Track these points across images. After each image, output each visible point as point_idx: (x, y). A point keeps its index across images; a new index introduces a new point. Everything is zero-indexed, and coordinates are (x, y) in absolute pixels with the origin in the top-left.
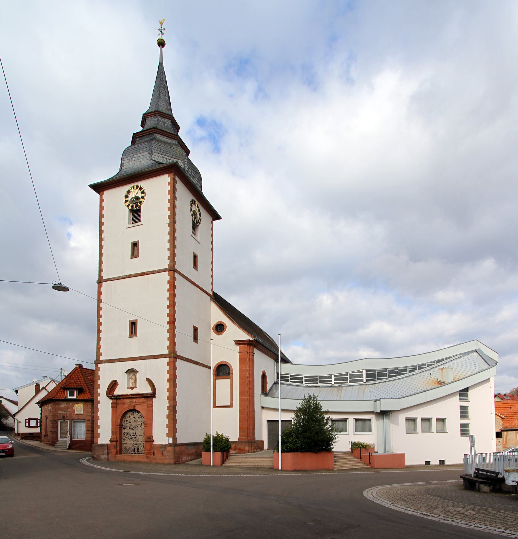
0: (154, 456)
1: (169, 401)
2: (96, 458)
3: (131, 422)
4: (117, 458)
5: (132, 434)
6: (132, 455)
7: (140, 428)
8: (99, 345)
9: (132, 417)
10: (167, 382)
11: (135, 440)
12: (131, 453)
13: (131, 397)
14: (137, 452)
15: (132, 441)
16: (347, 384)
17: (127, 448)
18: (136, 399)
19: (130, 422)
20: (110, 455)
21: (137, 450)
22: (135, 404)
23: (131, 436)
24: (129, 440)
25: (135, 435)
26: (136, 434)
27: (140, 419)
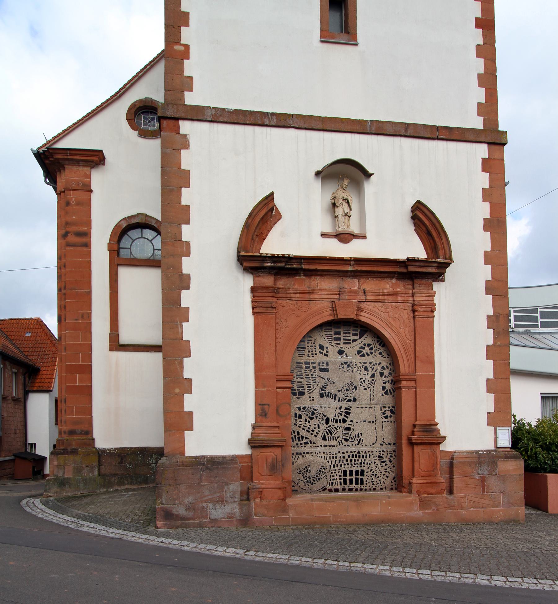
0: (451, 497)
2: (183, 519)
3: (326, 370)
4: (291, 514)
5: (331, 417)
6: (333, 499)
7: (368, 393)
8: (178, 42)
9: (333, 350)
11: (346, 440)
12: (330, 490)
13: (350, 268)
14: (354, 486)
15: (335, 443)
16: (538, 329)
17: (313, 472)
19: (321, 370)
20: (258, 500)
21: (354, 477)
22: (363, 297)
23: (327, 421)
24: (319, 440)
25: (344, 421)
26: (350, 417)
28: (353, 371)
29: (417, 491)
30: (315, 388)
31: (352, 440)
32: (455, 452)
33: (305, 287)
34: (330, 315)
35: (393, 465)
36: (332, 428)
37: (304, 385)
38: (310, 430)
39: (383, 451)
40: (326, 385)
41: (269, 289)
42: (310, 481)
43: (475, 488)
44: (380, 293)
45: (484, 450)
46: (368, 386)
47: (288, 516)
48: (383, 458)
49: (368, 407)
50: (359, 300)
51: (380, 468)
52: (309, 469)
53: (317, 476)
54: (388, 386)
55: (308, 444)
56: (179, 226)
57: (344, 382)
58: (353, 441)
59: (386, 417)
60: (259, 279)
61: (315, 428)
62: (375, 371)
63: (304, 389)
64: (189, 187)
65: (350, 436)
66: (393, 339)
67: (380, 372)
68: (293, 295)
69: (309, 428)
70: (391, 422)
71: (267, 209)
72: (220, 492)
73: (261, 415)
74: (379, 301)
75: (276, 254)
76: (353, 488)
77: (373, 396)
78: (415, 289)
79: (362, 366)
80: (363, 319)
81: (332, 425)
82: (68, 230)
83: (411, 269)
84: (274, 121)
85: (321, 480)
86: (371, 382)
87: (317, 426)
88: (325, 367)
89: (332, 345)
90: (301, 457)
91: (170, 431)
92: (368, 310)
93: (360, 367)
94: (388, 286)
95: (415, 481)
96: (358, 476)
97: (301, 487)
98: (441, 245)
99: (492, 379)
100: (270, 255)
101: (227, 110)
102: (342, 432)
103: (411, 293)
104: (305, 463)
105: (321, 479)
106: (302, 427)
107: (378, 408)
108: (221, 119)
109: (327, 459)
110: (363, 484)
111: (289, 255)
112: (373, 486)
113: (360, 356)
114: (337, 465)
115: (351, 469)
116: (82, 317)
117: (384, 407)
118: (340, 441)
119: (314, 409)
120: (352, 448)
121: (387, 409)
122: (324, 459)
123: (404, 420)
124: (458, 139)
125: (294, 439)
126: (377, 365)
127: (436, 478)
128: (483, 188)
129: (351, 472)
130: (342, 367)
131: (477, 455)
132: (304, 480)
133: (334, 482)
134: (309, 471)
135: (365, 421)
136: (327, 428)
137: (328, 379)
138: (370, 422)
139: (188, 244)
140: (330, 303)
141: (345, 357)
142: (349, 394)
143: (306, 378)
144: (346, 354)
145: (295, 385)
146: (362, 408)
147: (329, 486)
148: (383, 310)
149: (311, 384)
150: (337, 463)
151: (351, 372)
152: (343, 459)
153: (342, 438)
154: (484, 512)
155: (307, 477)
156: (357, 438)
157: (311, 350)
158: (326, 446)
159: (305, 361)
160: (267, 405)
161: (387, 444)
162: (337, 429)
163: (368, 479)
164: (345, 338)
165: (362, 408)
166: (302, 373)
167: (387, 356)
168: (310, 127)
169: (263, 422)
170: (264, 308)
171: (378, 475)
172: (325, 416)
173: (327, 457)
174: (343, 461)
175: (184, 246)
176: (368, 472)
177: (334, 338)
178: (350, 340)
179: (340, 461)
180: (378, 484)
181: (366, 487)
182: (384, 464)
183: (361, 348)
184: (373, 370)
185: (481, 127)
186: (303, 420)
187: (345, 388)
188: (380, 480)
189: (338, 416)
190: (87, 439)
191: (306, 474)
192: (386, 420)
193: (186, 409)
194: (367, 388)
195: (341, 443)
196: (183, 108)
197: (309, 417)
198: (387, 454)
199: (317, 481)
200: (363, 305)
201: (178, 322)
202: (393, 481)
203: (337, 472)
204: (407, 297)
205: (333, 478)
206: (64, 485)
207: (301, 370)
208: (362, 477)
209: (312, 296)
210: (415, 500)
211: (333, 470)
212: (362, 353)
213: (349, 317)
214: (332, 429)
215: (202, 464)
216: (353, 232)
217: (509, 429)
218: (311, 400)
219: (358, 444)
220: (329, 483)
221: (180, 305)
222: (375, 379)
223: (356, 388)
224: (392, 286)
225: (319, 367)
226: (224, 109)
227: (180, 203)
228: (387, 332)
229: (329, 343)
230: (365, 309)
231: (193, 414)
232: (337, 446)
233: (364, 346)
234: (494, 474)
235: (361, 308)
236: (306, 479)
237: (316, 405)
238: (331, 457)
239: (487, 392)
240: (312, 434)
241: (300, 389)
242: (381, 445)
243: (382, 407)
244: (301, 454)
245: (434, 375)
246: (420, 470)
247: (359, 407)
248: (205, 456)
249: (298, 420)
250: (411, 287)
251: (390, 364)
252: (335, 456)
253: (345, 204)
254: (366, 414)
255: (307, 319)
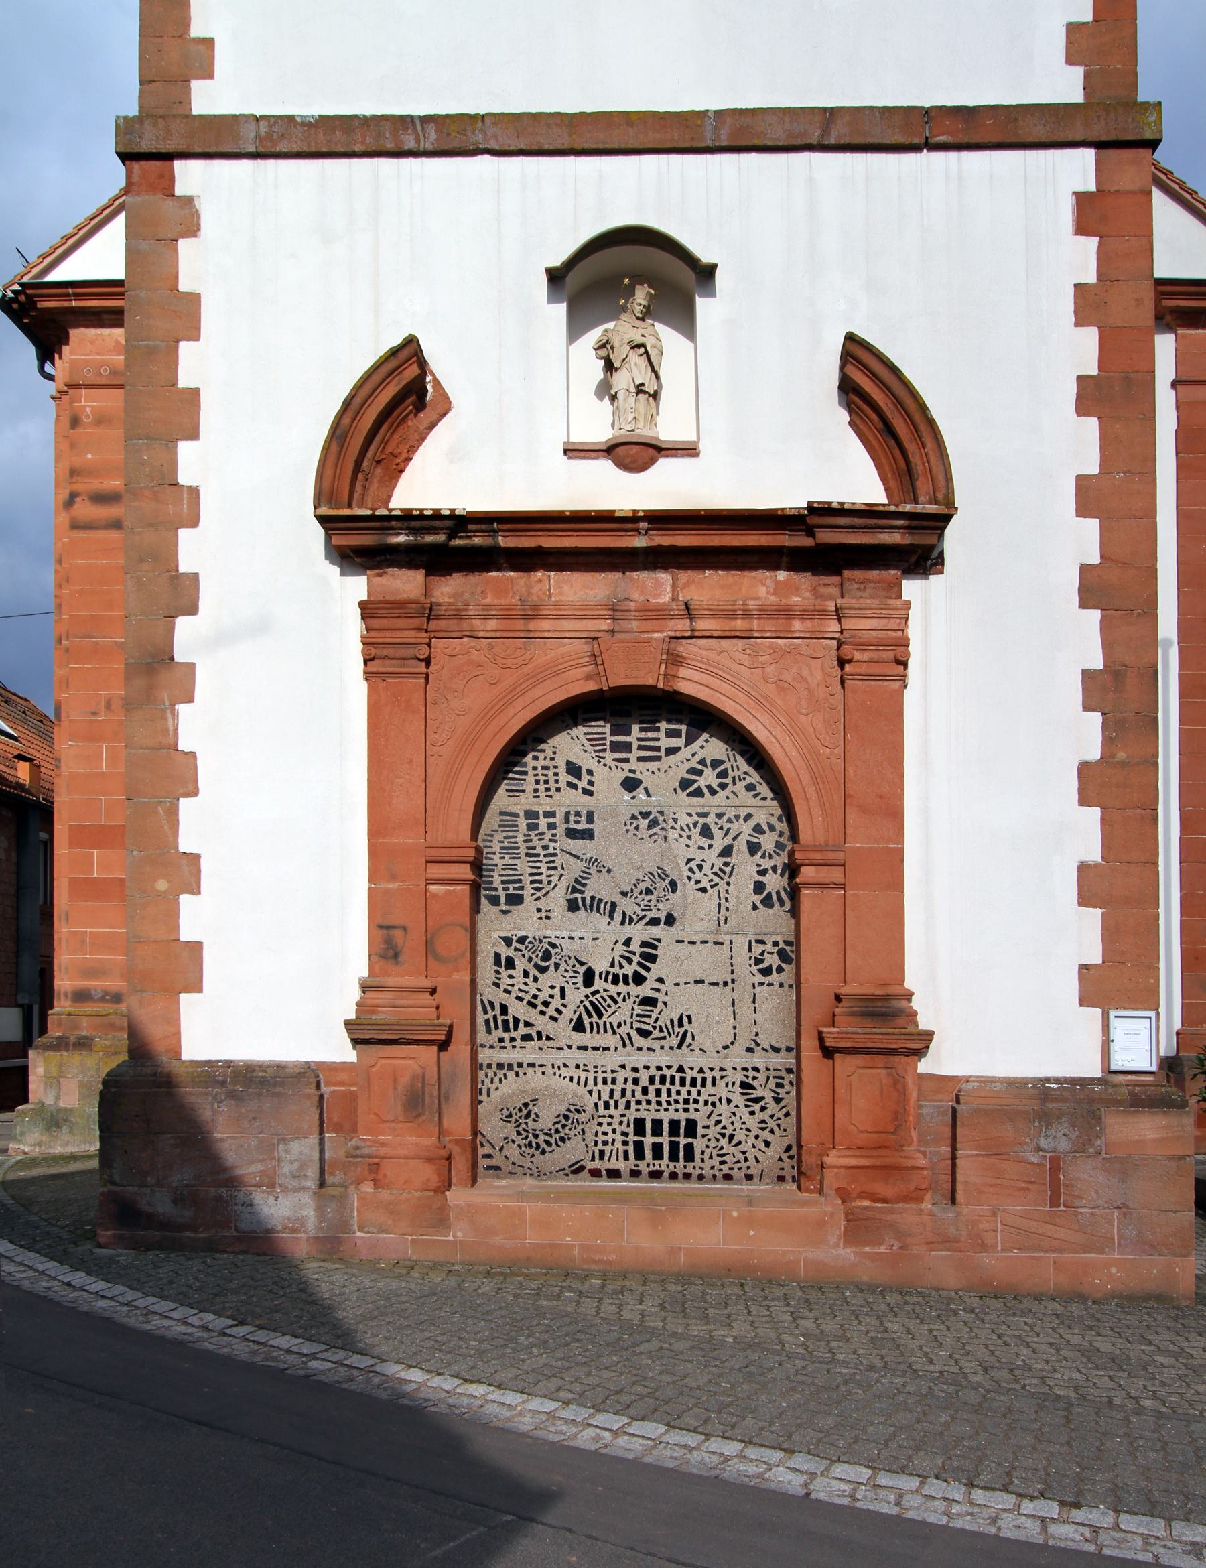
1: (1103, 620)
2: (165, 1224)
3: (588, 835)
4: (459, 1232)
5: (600, 966)
6: (601, 1195)
7: (710, 901)
10: (1083, 407)
11: (644, 1033)
12: (595, 1173)
13: (639, 542)
14: (664, 1164)
15: (611, 1040)
18: (684, 576)
19: (572, 834)
20: (368, 1188)
21: (665, 1140)
22: (683, 626)
24: (563, 1031)
25: (639, 980)
26: (657, 970)
27: (709, 802)
28: (665, 838)
29: (838, 1190)
30: (553, 884)
31: (662, 1034)
32: (968, 1080)
33: (515, 600)
34: (588, 677)
35: (784, 1110)
36: (602, 997)
37: (521, 875)
38: (538, 1002)
39: (756, 1069)
40: (585, 875)
41: (407, 608)
42: (538, 1145)
43: (1028, 1189)
44: (735, 611)
45: (1066, 1079)
46: (711, 880)
47: (451, 1238)
48: (753, 1088)
49: (711, 940)
50: (673, 634)
51: (746, 1117)
52: (535, 1110)
53: (557, 1131)
54: (774, 883)
55: (533, 1040)
56: (170, 445)
57: (638, 869)
58: (664, 1038)
59: (766, 972)
60: (383, 580)
61: (552, 997)
62: (735, 838)
63: (522, 888)
64: (198, 339)
65: (656, 1021)
66: (777, 744)
67: (748, 842)
68: (477, 624)
69: (535, 997)
70: (781, 985)
71: (399, 383)
72: (262, 1161)
73: (383, 957)
74: (733, 634)
75: (416, 510)
76: (663, 1172)
77: (727, 909)
78: (846, 596)
79: (695, 825)
80: (686, 688)
81: (601, 990)
82: (76, 487)
83: (827, 537)
84: (431, 138)
85: (568, 1144)
86: (720, 870)
87: (557, 992)
88: (583, 825)
89: (605, 765)
90: (511, 1075)
91: (142, 991)
92: (701, 662)
93: (688, 825)
94: (762, 591)
95: (830, 1160)
96: (678, 1136)
97: (512, 1159)
98: (923, 463)
99: (1097, 865)
100: (399, 513)
101: (299, 119)
102: (633, 1009)
103: (834, 609)
104: (522, 1092)
105: (569, 1139)
106: (515, 992)
107: (741, 944)
108: (283, 147)
109: (585, 1085)
110: (693, 1161)
111: (454, 510)
112: (722, 1167)
113: (688, 795)
114: (616, 1102)
115: (658, 1116)
116: (108, 705)
117: (759, 942)
118: (625, 1036)
119: (550, 944)
120: (660, 1056)
121: (769, 947)
122: (578, 1083)
123: (807, 980)
124: (995, 140)
125: (492, 1024)
126: (741, 820)
127: (903, 1154)
128: (1076, 286)
129: (657, 1126)
130: (635, 825)
131: (1037, 1092)
132: (518, 1139)
133: (608, 1149)
134: (533, 1116)
135: (702, 982)
136: (587, 997)
137: (591, 858)
138: (717, 984)
139: (194, 492)
140: (586, 643)
141: (642, 796)
142: (652, 904)
143: (527, 855)
144: (646, 789)
145: (496, 874)
146: (694, 943)
147: (593, 1159)
148: (745, 659)
149: (541, 874)
150: (615, 1098)
151: (660, 841)
152: (635, 1087)
153: (632, 1028)
154: (1055, 1263)
155: (527, 1131)
156: (677, 1029)
157: (542, 779)
158: (585, 1048)
159: (527, 808)
160: (400, 927)
161: (768, 1048)
162: (616, 1002)
163: (707, 1146)
164: (643, 743)
165: (693, 943)
166: (516, 843)
167: (770, 795)
168: (534, 147)
169: (389, 975)
170: (394, 662)
171: (740, 1136)
172: (582, 964)
173: (587, 1078)
174: (633, 1091)
175: (182, 500)
176: (707, 1127)
177: (611, 742)
178: (658, 749)
179: (624, 1091)
180: (739, 1162)
181: (701, 1168)
182: (757, 1107)
183: (693, 771)
184: (726, 834)
185: (1077, 96)
186: (518, 972)
187: (642, 886)
188: (744, 1152)
189: (620, 964)
190: (116, 1014)
191: (526, 1123)
192: (766, 980)
193: (186, 935)
194: (709, 888)
195: (627, 1042)
196: (182, 126)
197: (536, 966)
198: (768, 1078)
199: (558, 1145)
200: (684, 648)
201: (167, 703)
202: (784, 1156)
203: (616, 1121)
204: (823, 621)
205: (605, 1138)
206: (58, 1126)
207: (514, 834)
208: (690, 1140)
209: (532, 625)
210: (832, 1214)
211: (604, 1116)
212: (696, 786)
213: (640, 682)
214: (602, 1001)
215: (218, 1082)
216: (657, 439)
217: (1150, 1018)
218: (540, 918)
219: (680, 1046)
220: (591, 1153)
221: (172, 659)
222: (732, 860)
223: (673, 885)
224: (775, 589)
225: (566, 826)
226: (291, 118)
227: (174, 384)
228: (760, 726)
229: (597, 759)
230: (693, 659)
231: (202, 948)
232: (616, 1048)
233: (700, 767)
234: (1092, 1150)
235: (678, 656)
236: (527, 1137)
237: (557, 934)
238: (600, 1080)
239: (1080, 904)
240: (543, 1013)
241: (511, 886)
242: (749, 1050)
243: (753, 943)
244: (510, 1067)
245: (902, 850)
246: (853, 1127)
247: (682, 942)
248: (231, 1062)
249: (505, 974)
250: (835, 591)
251: (780, 819)
252: (609, 1076)
253: (636, 358)
254: (704, 961)
255: (518, 689)
